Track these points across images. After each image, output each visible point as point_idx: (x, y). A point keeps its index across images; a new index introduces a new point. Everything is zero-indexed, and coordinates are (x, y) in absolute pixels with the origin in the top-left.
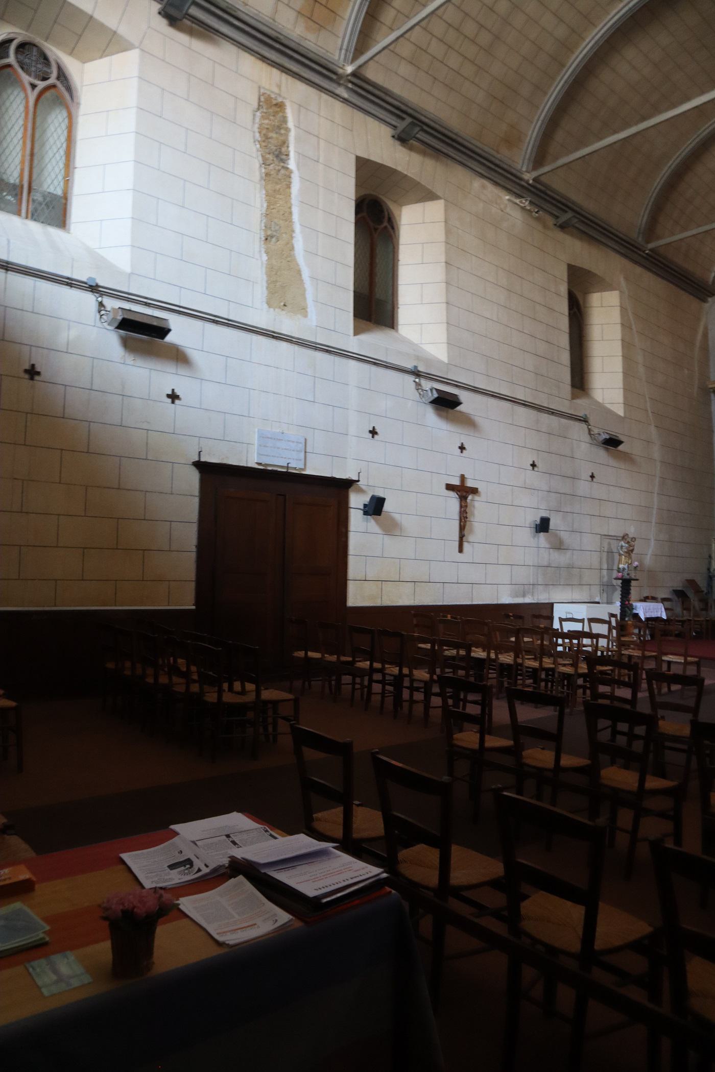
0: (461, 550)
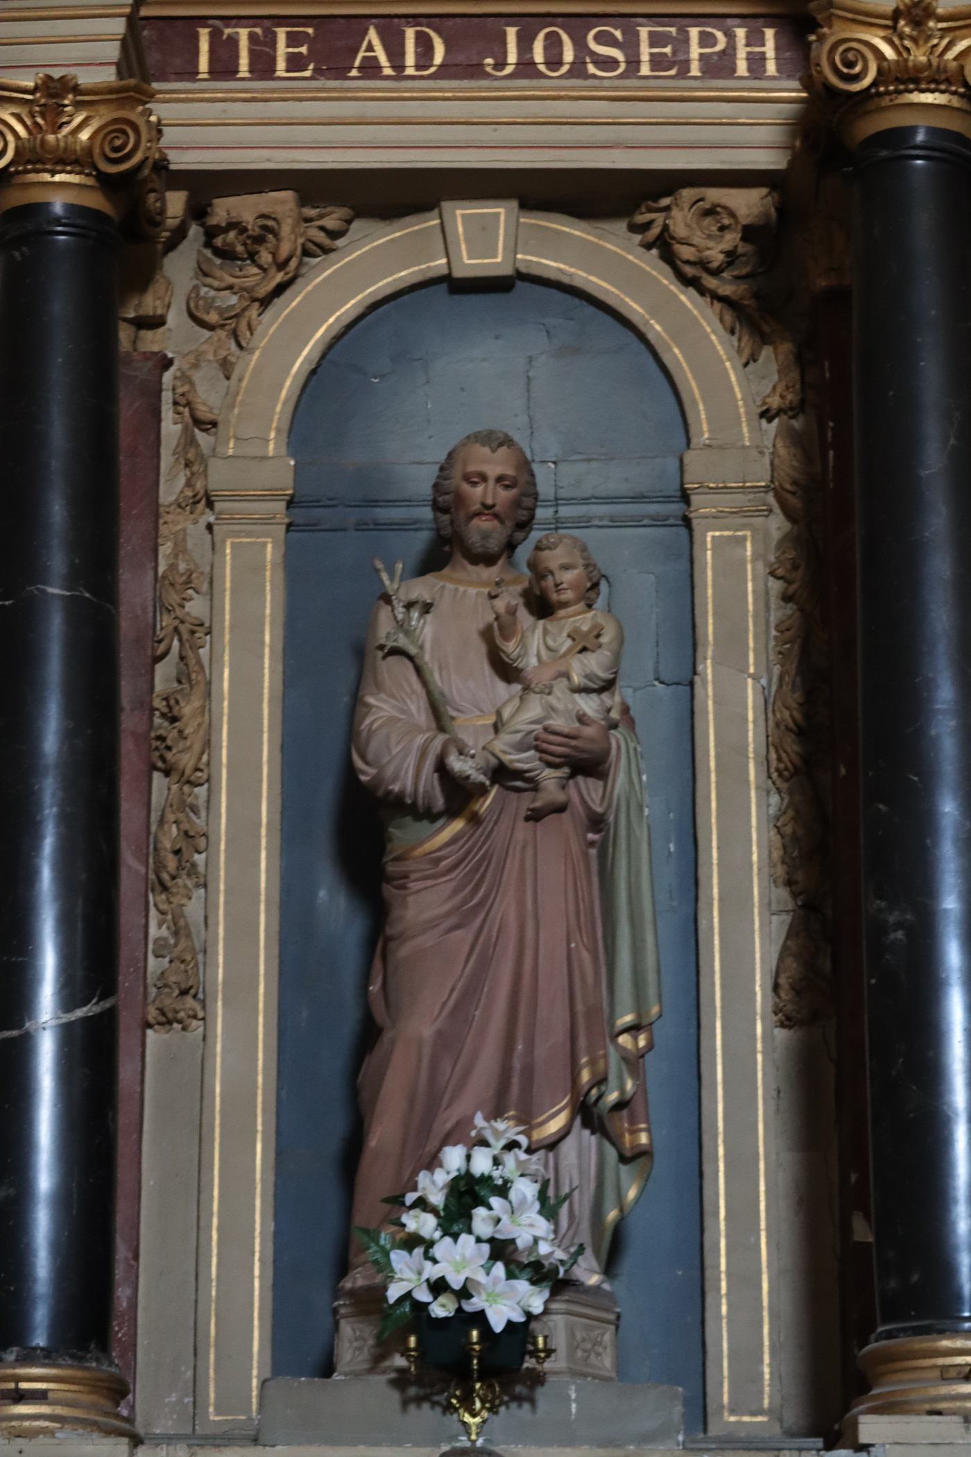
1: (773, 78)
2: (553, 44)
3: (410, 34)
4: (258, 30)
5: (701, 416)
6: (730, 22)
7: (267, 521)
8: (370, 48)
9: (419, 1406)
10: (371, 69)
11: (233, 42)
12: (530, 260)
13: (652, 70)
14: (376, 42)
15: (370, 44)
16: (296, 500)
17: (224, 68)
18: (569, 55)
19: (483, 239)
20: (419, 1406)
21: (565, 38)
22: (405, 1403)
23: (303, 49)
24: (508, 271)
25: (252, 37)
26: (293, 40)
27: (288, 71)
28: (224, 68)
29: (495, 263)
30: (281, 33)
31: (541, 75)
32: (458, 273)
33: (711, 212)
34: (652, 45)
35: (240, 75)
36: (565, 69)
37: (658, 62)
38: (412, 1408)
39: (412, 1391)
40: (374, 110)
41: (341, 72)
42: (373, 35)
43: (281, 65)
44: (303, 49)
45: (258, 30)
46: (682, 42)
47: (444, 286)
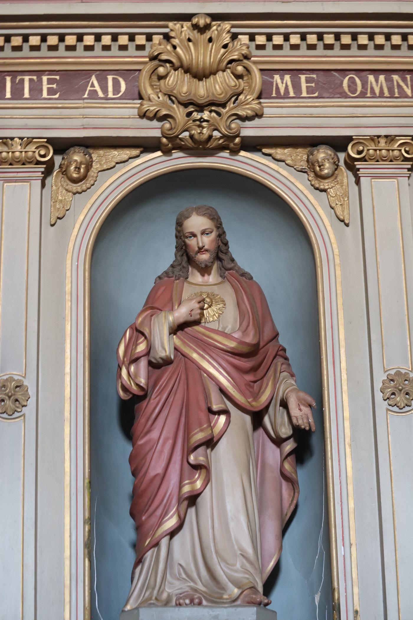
0: (347, 225)
1: (8, 99)
2: (352, 82)
3: (110, 78)
4: (35, 78)
6: (364, 74)
8: (93, 85)
10: (93, 95)
13: (307, 94)
14: (96, 83)
15: (92, 83)
17: (17, 93)
18: (359, 88)
21: (357, 80)
23: (54, 86)
25: (31, 80)
27: (114, 95)
28: (17, 93)
30: (45, 78)
34: (48, 84)
35: (385, 95)
36: (358, 93)
40: (285, 111)
42: (94, 79)
43: (45, 94)
44: (54, 86)
45: (35, 78)
46: (40, 81)
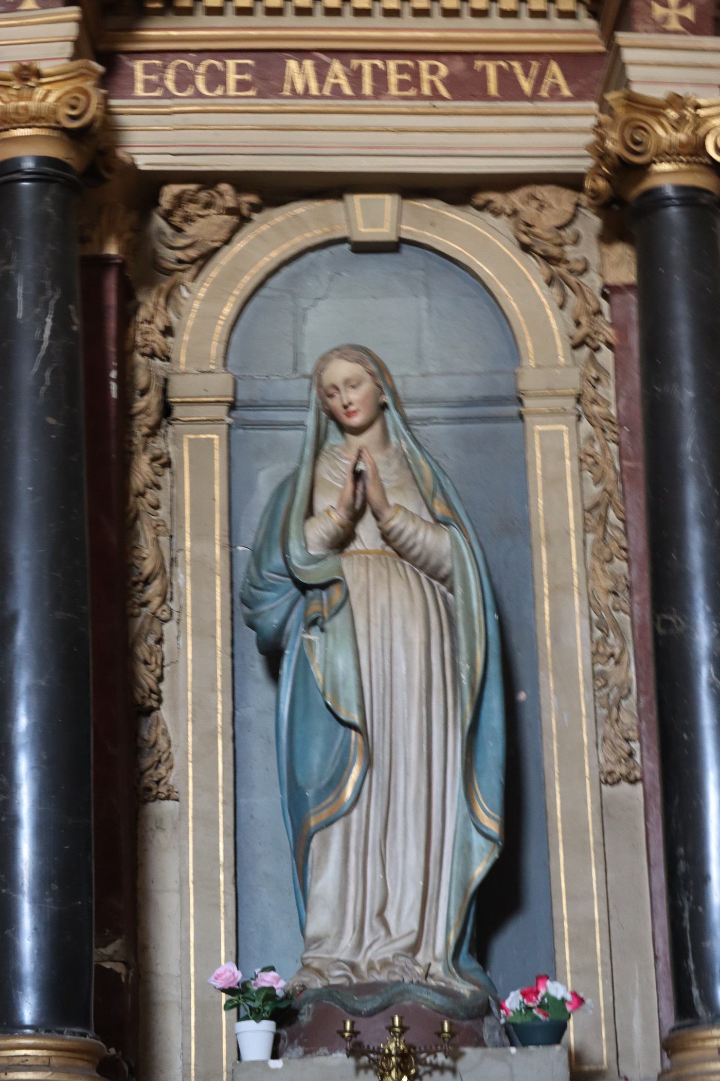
5: (528, 344)
7: (563, 412)
9: (366, 1072)
11: (359, 71)
12: (410, 231)
13: (146, 91)
16: (238, 404)
19: (373, 217)
20: (366, 1072)
22: (358, 1068)
24: (393, 238)
26: (241, 69)
29: (384, 232)
31: (174, 97)
32: (356, 238)
33: (534, 198)
37: (402, 85)
38: (362, 1072)
39: (364, 1060)
41: (276, 92)
45: (503, 64)
47: (347, 247)
